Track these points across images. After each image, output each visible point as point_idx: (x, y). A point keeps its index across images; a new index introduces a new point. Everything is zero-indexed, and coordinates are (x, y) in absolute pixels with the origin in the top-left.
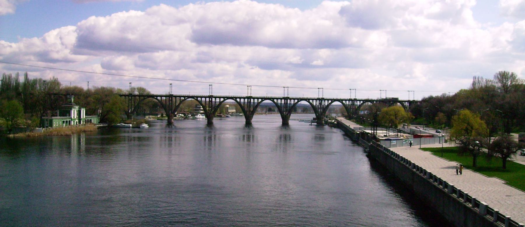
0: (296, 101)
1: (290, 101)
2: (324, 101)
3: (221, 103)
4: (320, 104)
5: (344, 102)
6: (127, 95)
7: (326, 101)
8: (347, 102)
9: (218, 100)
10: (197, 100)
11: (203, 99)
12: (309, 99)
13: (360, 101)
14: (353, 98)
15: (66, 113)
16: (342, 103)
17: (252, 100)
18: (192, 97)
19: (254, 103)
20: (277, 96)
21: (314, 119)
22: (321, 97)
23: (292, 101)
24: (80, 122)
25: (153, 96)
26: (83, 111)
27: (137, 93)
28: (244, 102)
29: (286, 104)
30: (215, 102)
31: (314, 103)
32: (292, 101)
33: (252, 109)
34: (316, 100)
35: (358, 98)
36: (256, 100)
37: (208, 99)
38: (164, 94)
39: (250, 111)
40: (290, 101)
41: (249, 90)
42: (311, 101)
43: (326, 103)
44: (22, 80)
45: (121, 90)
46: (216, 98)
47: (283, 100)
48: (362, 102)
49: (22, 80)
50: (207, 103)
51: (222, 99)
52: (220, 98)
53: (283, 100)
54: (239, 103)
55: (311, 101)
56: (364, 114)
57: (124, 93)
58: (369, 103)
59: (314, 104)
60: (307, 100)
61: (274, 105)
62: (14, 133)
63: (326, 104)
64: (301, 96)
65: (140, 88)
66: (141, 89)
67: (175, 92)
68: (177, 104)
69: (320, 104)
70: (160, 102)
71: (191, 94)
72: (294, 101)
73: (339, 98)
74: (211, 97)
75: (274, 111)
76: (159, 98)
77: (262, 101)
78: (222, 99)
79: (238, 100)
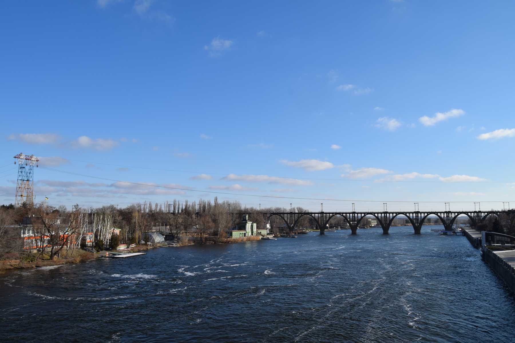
0: (426, 214)
2: (451, 214)
3: (362, 217)
5: (469, 214)
6: (289, 213)
8: (473, 214)
9: (423, 215)
10: (343, 215)
11: (380, 215)
13: (484, 212)
14: (477, 210)
15: (242, 227)
17: (356, 215)
18: (339, 213)
20: (409, 211)
22: (448, 210)
24: (252, 234)
25: (308, 213)
26: (255, 225)
27: (297, 211)
28: (381, 217)
29: (448, 216)
31: (442, 215)
32: (391, 215)
34: (444, 213)
35: (482, 210)
36: (423, 215)
37: (383, 215)
38: (317, 211)
39: (386, 224)
41: (385, 207)
43: (453, 215)
44: (213, 203)
46: (358, 213)
48: (486, 214)
49: (213, 203)
50: (351, 217)
51: (395, 215)
52: (361, 213)
53: (414, 214)
54: (377, 217)
57: (286, 212)
59: (411, 217)
60: (436, 213)
62: (122, 272)
63: (453, 216)
64: (430, 211)
66: (299, 209)
67: (326, 209)
68: (327, 219)
71: (338, 211)
73: (434, 211)
74: (354, 213)
75: (143, 215)
76: (313, 215)
77: (396, 215)
78: (363, 215)
79: (376, 215)
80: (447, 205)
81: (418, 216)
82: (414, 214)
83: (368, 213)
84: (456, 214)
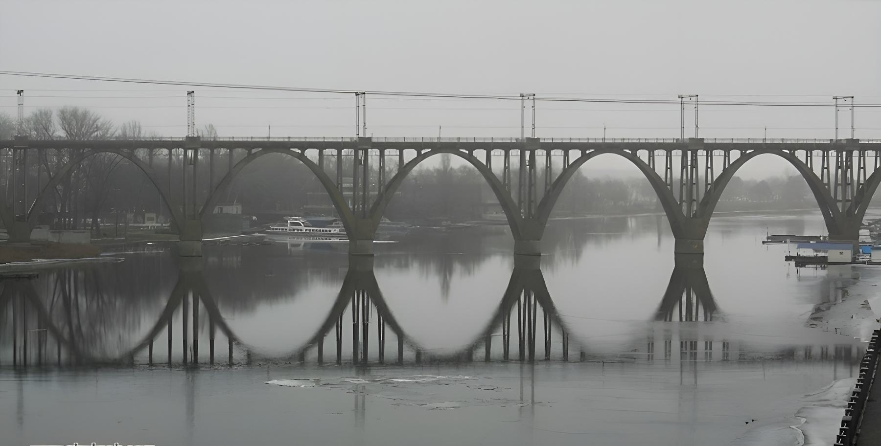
0: (575, 155)
1: (709, 156)
4: (845, 167)
7: (718, 154)
12: (636, 147)
16: (470, 158)
19: (549, 167)
21: (581, 234)
23: (718, 154)
27: (59, 132)
30: (549, 167)
32: (557, 156)
33: (702, 195)
34: (825, 148)
36: (557, 156)
40: (709, 156)
41: (528, 112)
42: (801, 155)
45: (136, 126)
47: (833, 153)
50: (347, 166)
51: (410, 155)
55: (643, 155)
56: (521, 213)
58: (457, 162)
59: (817, 171)
60: (626, 149)
61: (642, 175)
65: (74, 114)
66: (72, 118)
69: (845, 167)
70: (317, 169)
72: (727, 156)
76: (312, 154)
78: (410, 155)
80: (690, 110)
81: (694, 165)
82: (677, 154)
83: (761, 148)
84: (735, 155)
